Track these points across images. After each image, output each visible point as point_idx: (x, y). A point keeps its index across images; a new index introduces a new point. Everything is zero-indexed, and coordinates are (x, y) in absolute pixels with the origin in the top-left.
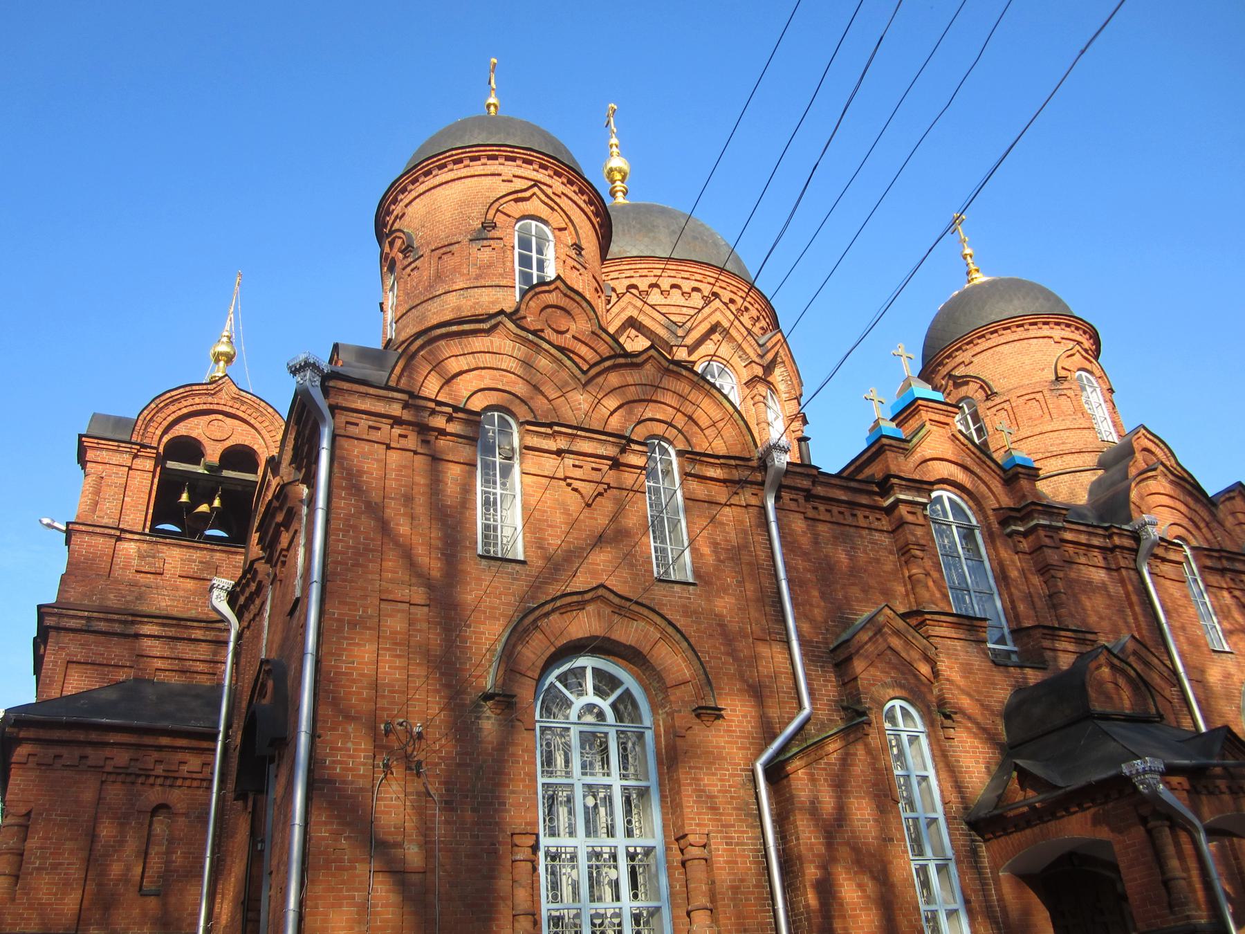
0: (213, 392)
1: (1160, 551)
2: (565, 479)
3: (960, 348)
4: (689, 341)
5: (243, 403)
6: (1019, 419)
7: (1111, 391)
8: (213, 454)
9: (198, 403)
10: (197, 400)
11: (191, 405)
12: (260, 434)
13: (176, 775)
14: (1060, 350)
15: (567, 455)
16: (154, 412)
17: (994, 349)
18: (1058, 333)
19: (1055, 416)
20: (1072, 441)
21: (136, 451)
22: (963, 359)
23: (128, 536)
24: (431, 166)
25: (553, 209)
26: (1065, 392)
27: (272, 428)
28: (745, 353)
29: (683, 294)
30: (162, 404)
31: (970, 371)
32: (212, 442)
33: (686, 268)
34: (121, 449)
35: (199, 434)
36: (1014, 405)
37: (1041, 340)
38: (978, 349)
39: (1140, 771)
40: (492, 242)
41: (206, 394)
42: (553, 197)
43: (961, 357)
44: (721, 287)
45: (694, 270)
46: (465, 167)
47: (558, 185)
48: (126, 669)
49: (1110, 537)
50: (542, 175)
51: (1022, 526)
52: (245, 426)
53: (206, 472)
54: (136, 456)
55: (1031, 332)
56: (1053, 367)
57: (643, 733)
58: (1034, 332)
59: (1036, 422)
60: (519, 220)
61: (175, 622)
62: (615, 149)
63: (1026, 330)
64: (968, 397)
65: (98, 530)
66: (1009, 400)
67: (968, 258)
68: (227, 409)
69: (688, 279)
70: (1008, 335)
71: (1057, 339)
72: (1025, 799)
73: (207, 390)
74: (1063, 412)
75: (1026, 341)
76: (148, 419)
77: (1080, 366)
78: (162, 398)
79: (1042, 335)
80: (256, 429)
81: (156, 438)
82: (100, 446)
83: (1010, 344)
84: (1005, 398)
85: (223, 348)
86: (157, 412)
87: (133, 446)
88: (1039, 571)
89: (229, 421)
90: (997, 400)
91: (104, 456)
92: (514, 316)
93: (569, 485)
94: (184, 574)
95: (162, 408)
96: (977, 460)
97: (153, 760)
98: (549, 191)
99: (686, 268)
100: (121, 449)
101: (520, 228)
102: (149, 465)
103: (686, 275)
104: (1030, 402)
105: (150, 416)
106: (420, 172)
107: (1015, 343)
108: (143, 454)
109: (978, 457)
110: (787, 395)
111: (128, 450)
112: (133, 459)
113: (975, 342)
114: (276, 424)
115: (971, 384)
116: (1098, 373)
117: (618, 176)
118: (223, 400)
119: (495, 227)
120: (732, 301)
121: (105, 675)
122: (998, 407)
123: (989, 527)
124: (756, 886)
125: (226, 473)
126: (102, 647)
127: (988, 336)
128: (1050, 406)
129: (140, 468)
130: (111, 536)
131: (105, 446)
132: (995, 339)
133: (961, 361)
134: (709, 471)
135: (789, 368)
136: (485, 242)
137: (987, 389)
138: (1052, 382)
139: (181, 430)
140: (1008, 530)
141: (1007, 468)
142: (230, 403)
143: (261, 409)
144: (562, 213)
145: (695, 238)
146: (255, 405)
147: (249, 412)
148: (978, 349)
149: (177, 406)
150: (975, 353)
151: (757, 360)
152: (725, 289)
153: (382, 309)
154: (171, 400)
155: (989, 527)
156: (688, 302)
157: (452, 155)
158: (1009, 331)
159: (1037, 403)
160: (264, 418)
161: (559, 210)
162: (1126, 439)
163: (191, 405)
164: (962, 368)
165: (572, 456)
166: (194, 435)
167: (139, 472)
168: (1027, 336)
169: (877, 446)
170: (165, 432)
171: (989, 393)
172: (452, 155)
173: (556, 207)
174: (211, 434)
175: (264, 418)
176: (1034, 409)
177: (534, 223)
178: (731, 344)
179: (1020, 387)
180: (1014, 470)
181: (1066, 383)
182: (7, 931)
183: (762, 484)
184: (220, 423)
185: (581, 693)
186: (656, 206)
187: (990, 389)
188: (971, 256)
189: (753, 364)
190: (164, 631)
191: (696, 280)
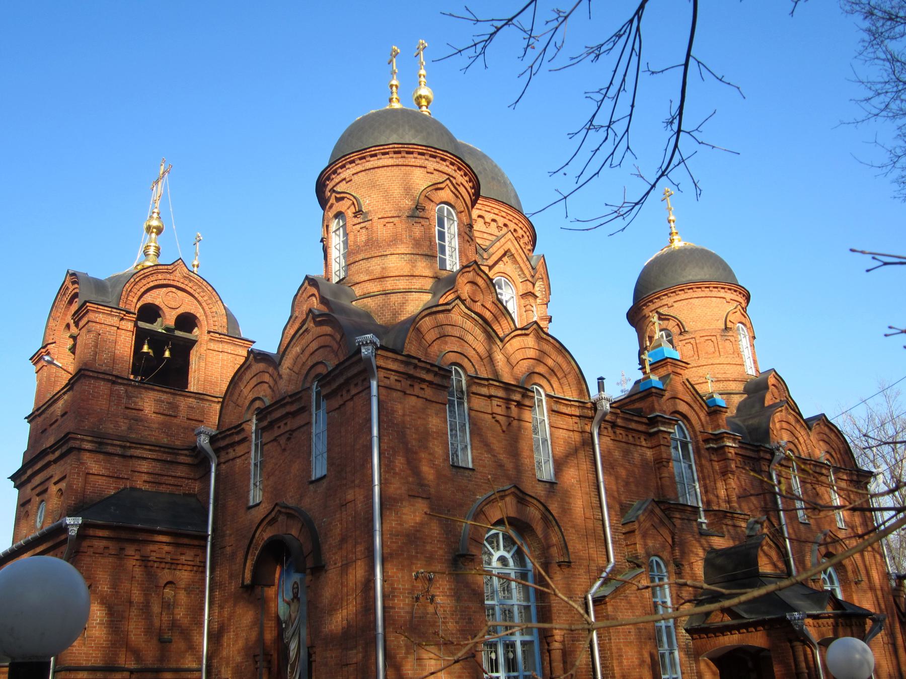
0: (171, 271)
1: (784, 462)
2: (492, 414)
3: (666, 295)
4: (490, 262)
5: (191, 281)
6: (700, 352)
7: (754, 338)
8: (169, 318)
9: (161, 279)
10: (160, 276)
11: (156, 280)
12: (201, 304)
13: (178, 562)
14: (731, 307)
15: (494, 398)
16: (133, 284)
17: (689, 300)
18: (729, 295)
19: (722, 354)
20: (730, 372)
21: (122, 315)
22: (667, 303)
23: (120, 381)
24: (378, 152)
25: (457, 197)
26: (730, 338)
27: (209, 302)
28: (524, 273)
29: (485, 223)
30: (138, 279)
31: (671, 312)
32: (169, 310)
33: (489, 204)
34: (113, 313)
35: (160, 302)
36: (698, 341)
37: (718, 299)
38: (678, 298)
39: (797, 618)
40: (421, 220)
41: (166, 272)
43: (665, 300)
44: (509, 220)
45: (494, 206)
46: (402, 157)
47: (463, 180)
48: (124, 481)
49: (758, 451)
50: (450, 170)
51: (715, 444)
52: (191, 298)
53: (164, 331)
54: (122, 319)
55: (713, 293)
56: (724, 319)
57: (527, 573)
58: (715, 293)
59: (710, 356)
60: (438, 205)
61: (157, 449)
62: (422, 79)
63: (710, 291)
64: (667, 330)
65: (101, 376)
66: (695, 338)
67: (394, 88)
68: (179, 285)
69: (489, 212)
70: (699, 293)
71: (728, 300)
72: (722, 621)
73: (167, 269)
74: (727, 352)
75: (709, 298)
76: (129, 290)
77: (739, 320)
78: (138, 275)
79: (720, 296)
80: (198, 301)
81: (133, 305)
82: (99, 310)
83: (699, 299)
84: (692, 336)
85: (155, 223)
86: (134, 285)
87: (121, 312)
88: (722, 473)
89: (180, 293)
90: (687, 336)
91: (100, 317)
93: (494, 418)
94: (157, 411)
95: (138, 282)
96: (694, 399)
97: (164, 552)
98: (454, 181)
99: (489, 204)
100: (113, 313)
102: (130, 326)
103: (488, 209)
104: (707, 342)
105: (130, 288)
106: (368, 154)
107: (703, 299)
108: (127, 318)
109: (693, 394)
110: (541, 301)
111: (118, 314)
112: (120, 320)
113: (677, 293)
114: (214, 299)
115: (671, 321)
116: (748, 325)
118: (177, 277)
119: (424, 209)
120: (515, 230)
121: (111, 484)
122: (687, 341)
123: (697, 442)
124: (586, 665)
125: (179, 333)
126: (110, 463)
127: (686, 291)
128: (720, 347)
129: (124, 328)
130: (108, 380)
131: (102, 311)
132: (690, 293)
133: (665, 303)
134: (563, 409)
135: (545, 283)
136: (417, 219)
137: (681, 327)
138: (723, 330)
139: (148, 299)
140: (708, 446)
141: (711, 406)
142: (182, 280)
143: (203, 287)
144: (462, 200)
145: (493, 178)
146: (199, 283)
147: (194, 288)
148: (678, 298)
149: (147, 280)
150: (676, 300)
151: (530, 279)
152: (511, 221)
154: (144, 276)
155: (697, 442)
156: (487, 229)
157: (394, 148)
158: (700, 289)
159: (711, 343)
160: (204, 294)
161: (461, 198)
162: (763, 376)
163: (156, 280)
164: (666, 308)
165: (496, 399)
166: (157, 303)
167: (123, 331)
168: (711, 295)
169: (648, 392)
170: (139, 300)
171: (683, 331)
172: (394, 148)
173: (459, 196)
174: (168, 303)
175: (204, 294)
176: (710, 347)
177: (446, 206)
178: (514, 265)
179: (703, 330)
180: (715, 408)
181: (731, 332)
182: (84, 665)
183: (592, 418)
184: (174, 294)
185: (498, 549)
186: (468, 146)
187: (684, 328)
188: (674, 222)
189: (528, 282)
190: (150, 454)
191: (494, 214)
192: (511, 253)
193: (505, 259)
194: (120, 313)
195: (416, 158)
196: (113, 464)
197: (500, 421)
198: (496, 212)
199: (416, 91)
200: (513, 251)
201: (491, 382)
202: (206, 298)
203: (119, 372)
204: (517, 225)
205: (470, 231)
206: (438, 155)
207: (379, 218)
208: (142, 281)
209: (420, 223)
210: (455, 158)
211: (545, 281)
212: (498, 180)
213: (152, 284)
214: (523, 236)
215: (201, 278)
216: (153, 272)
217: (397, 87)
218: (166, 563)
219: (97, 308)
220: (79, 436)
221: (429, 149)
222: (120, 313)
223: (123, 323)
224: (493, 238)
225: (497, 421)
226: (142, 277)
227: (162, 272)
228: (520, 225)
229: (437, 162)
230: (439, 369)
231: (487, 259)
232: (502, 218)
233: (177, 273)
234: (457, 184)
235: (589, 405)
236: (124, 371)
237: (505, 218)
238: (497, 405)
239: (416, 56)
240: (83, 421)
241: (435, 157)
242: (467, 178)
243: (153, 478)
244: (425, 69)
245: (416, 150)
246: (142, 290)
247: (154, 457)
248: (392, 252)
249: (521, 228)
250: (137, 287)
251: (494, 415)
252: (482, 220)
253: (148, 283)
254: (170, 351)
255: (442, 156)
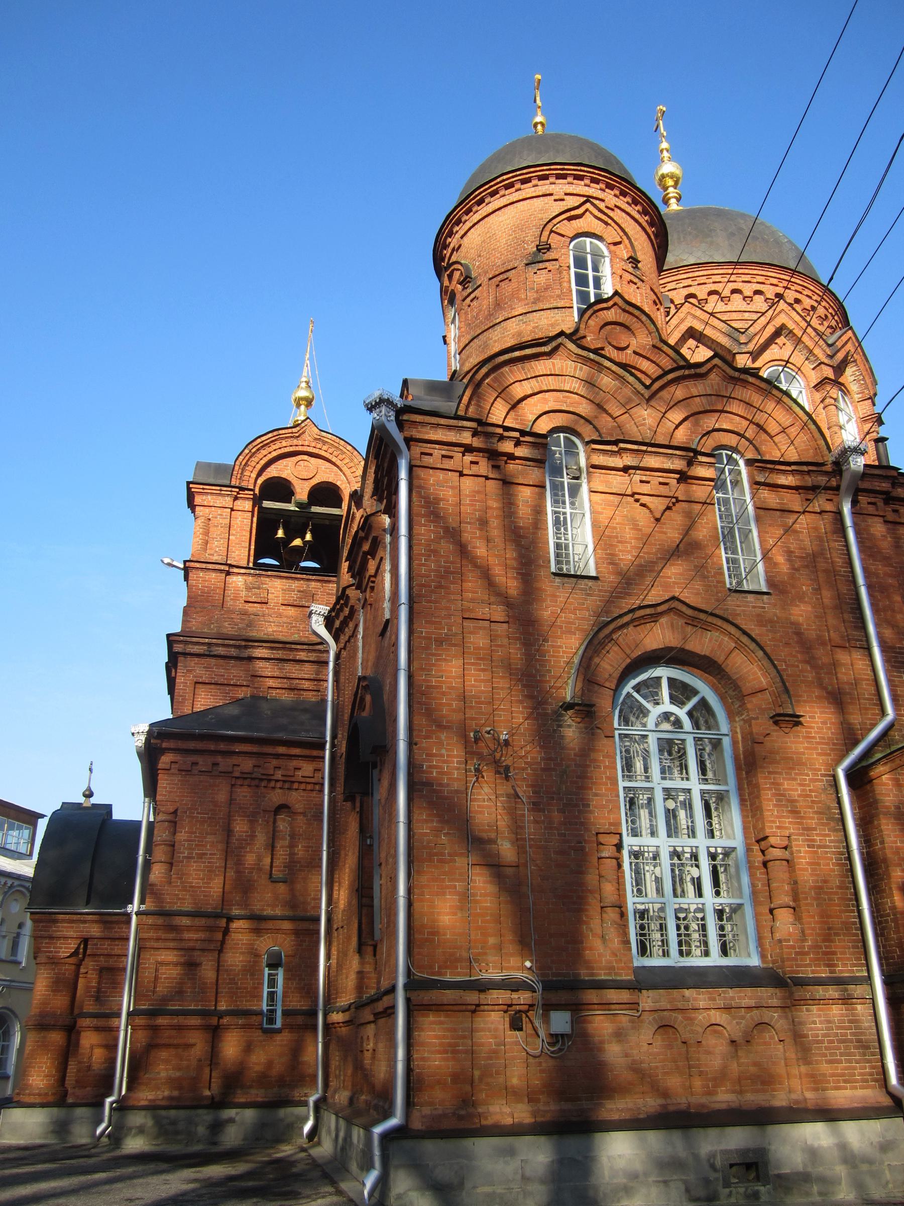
0: (297, 435)
2: (632, 495)
5: (325, 443)
8: (302, 492)
9: (286, 446)
10: (284, 443)
11: (280, 448)
12: (341, 470)
21: (235, 494)
24: (484, 194)
25: (606, 223)
27: (352, 464)
29: (745, 298)
33: (746, 271)
34: (223, 492)
40: (547, 264)
41: (292, 437)
42: (606, 211)
45: (755, 272)
52: (328, 464)
53: (297, 509)
54: (236, 498)
60: (573, 239)
61: (281, 645)
62: (665, 154)
65: (210, 566)
69: (749, 282)
73: (292, 433)
80: (338, 467)
81: (252, 481)
82: (205, 491)
85: (303, 393)
86: (251, 457)
87: (233, 489)
89: (313, 460)
92: (574, 336)
93: (637, 501)
95: (255, 453)
98: (602, 206)
99: (746, 271)
100: (223, 492)
101: (574, 247)
102: (248, 505)
108: (242, 496)
110: (860, 396)
111: (229, 493)
112: (234, 500)
117: (670, 182)
118: (307, 442)
120: (797, 301)
125: (315, 509)
126: (223, 669)
129: (240, 508)
130: (221, 571)
131: (209, 491)
134: (780, 479)
136: (540, 264)
139: (273, 472)
142: (313, 444)
144: (616, 227)
146: (335, 444)
147: (330, 451)
149: (268, 450)
151: (826, 361)
153: (445, 342)
154: (262, 444)
156: (749, 306)
160: (344, 456)
161: (613, 224)
163: (280, 448)
170: (259, 474)
173: (610, 221)
175: (344, 456)
182: (167, 909)
183: (837, 488)
184: (306, 462)
189: (822, 366)
190: (273, 653)
192: (788, 329)
193: (781, 340)
194: (231, 491)
195: (537, 186)
196: (228, 669)
197: (648, 504)
198: (760, 281)
199: (657, 173)
200: (791, 325)
201: (622, 445)
202: (347, 461)
203: (235, 561)
204: (801, 293)
205: (636, 267)
206: (569, 172)
207: (490, 279)
208: (262, 451)
209: (546, 268)
210: (597, 172)
211: (862, 367)
212: (763, 239)
213: (274, 454)
214: (826, 316)
215: (337, 437)
216: (273, 439)
217: (542, 124)
218: (277, 781)
219: (203, 489)
220: (182, 638)
221: (552, 167)
222: (231, 491)
223: (238, 502)
224: (755, 316)
225: (643, 505)
226: (259, 446)
227: (287, 438)
228: (805, 293)
229: (569, 183)
230: (504, 431)
231: (746, 344)
232: (772, 287)
233: (306, 436)
234: (607, 207)
235: (829, 468)
236: (242, 559)
237: (777, 286)
238: (642, 482)
239: (656, 131)
240: (189, 621)
241: (564, 177)
242: (628, 199)
243: (278, 683)
244: (666, 141)
245: (534, 175)
246: (263, 462)
247: (278, 656)
248: (507, 315)
249: (807, 296)
250: (255, 459)
251: (637, 497)
252: (741, 296)
253: (270, 453)
254: (312, 533)
255: (575, 172)
